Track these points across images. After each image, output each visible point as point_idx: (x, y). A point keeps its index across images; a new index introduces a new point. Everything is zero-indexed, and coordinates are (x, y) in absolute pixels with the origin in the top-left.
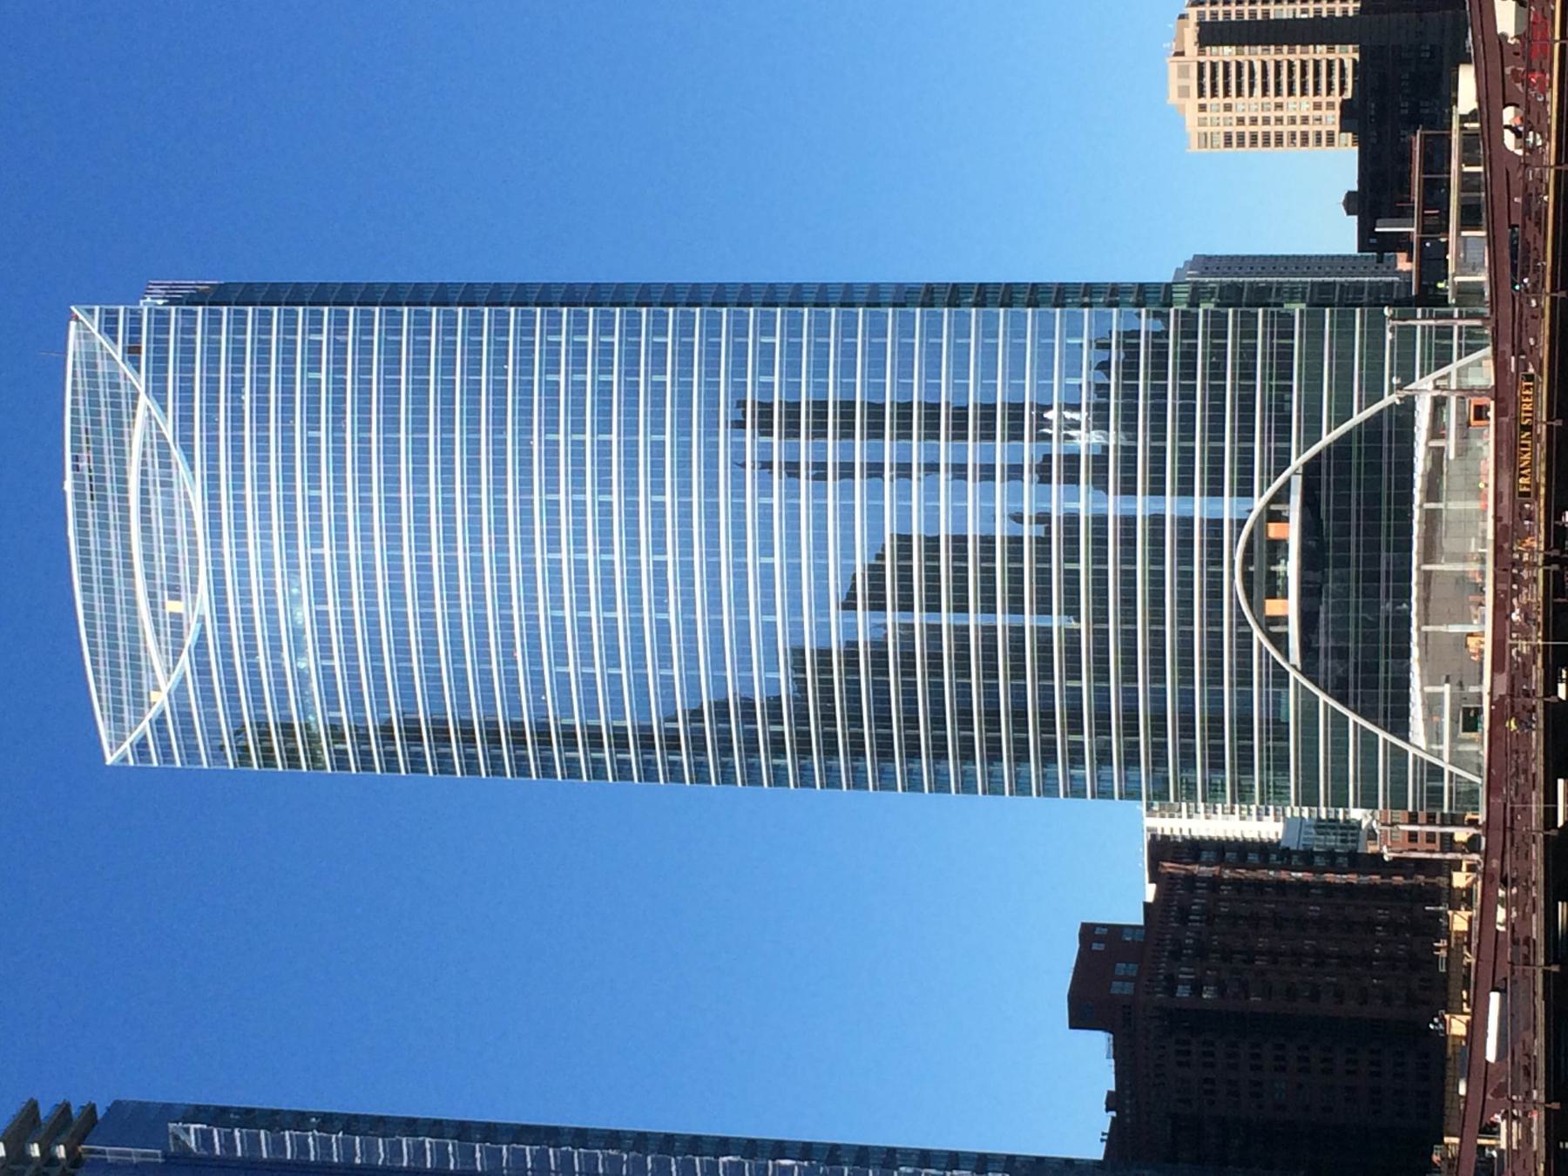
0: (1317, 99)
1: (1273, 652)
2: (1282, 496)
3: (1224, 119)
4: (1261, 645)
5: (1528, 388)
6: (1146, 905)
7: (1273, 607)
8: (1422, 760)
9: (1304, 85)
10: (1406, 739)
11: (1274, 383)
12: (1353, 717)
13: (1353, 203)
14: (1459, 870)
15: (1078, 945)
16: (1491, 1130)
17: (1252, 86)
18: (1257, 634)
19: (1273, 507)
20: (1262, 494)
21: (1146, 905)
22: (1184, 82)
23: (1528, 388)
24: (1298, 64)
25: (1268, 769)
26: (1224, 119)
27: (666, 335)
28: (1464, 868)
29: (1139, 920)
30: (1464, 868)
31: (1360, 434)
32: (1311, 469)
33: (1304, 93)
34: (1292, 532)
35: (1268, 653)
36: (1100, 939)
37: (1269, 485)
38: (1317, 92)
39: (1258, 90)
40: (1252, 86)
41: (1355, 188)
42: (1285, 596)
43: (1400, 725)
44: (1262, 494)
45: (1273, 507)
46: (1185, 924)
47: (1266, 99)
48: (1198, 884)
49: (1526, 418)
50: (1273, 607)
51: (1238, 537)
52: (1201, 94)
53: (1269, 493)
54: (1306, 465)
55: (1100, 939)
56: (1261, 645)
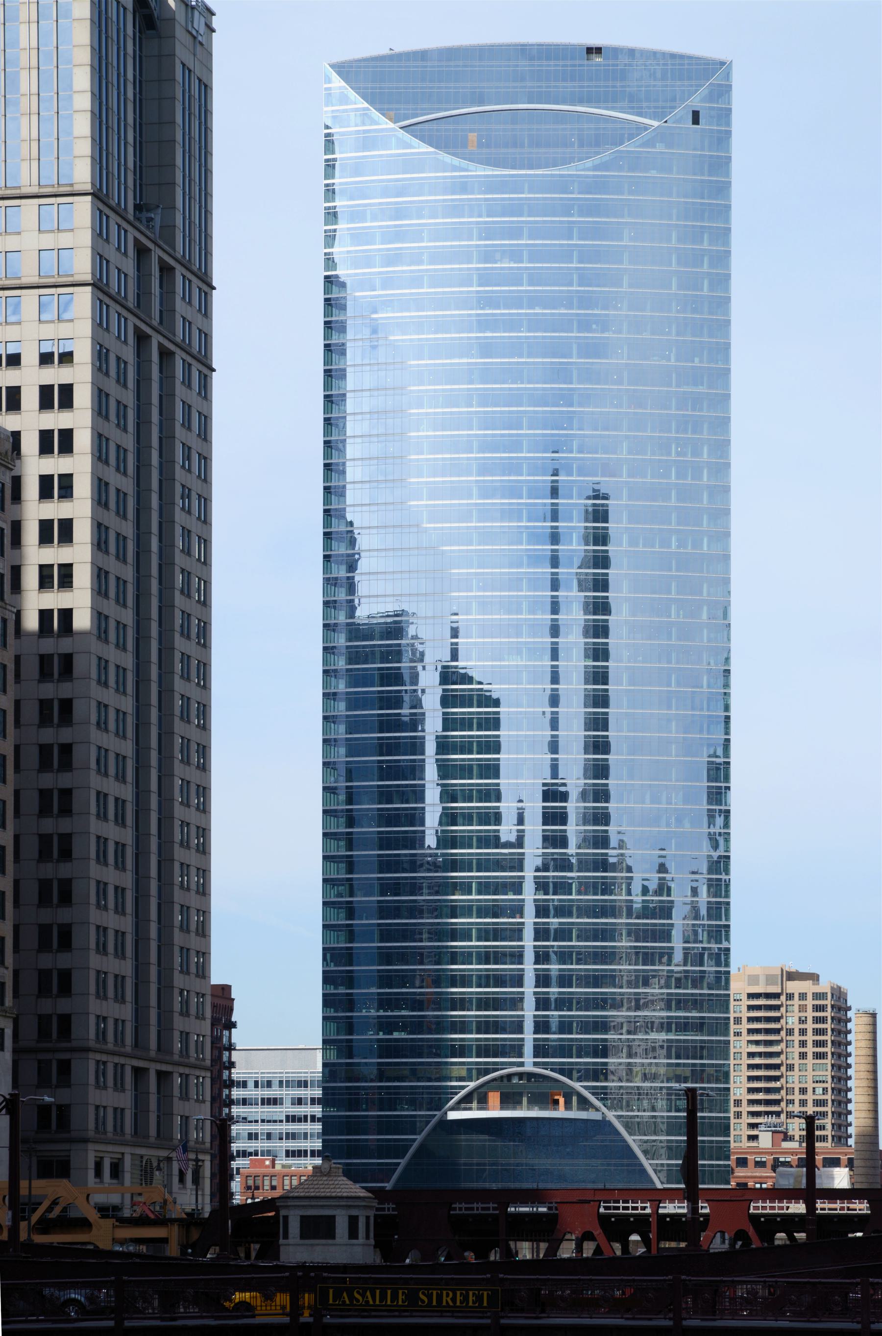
0: (745, 1103)
1: (457, 1098)
2: (584, 1103)
4: (463, 1087)
5: (479, 1298)
7: (494, 1098)
9: (757, 1090)
11: (673, 1097)
12: (403, 1162)
16: (618, 1290)
17: (757, 1043)
18: (472, 1085)
19: (575, 1099)
20: (586, 1088)
22: (762, 980)
23: (479, 1298)
24: (778, 1084)
25: (350, 1094)
27: (677, 570)
31: (635, 1165)
32: (604, 1125)
33: (751, 1090)
34: (561, 1113)
35: (456, 1094)
37: (593, 1094)
38: (751, 1102)
39: (754, 1049)
40: (757, 1043)
42: (502, 1108)
44: (586, 1088)
45: (575, 1099)
47: (745, 1056)
49: (430, 1297)
50: (494, 1098)
51: (552, 1070)
52: (751, 996)
53: (586, 1094)
54: (610, 1124)
56: (463, 1087)
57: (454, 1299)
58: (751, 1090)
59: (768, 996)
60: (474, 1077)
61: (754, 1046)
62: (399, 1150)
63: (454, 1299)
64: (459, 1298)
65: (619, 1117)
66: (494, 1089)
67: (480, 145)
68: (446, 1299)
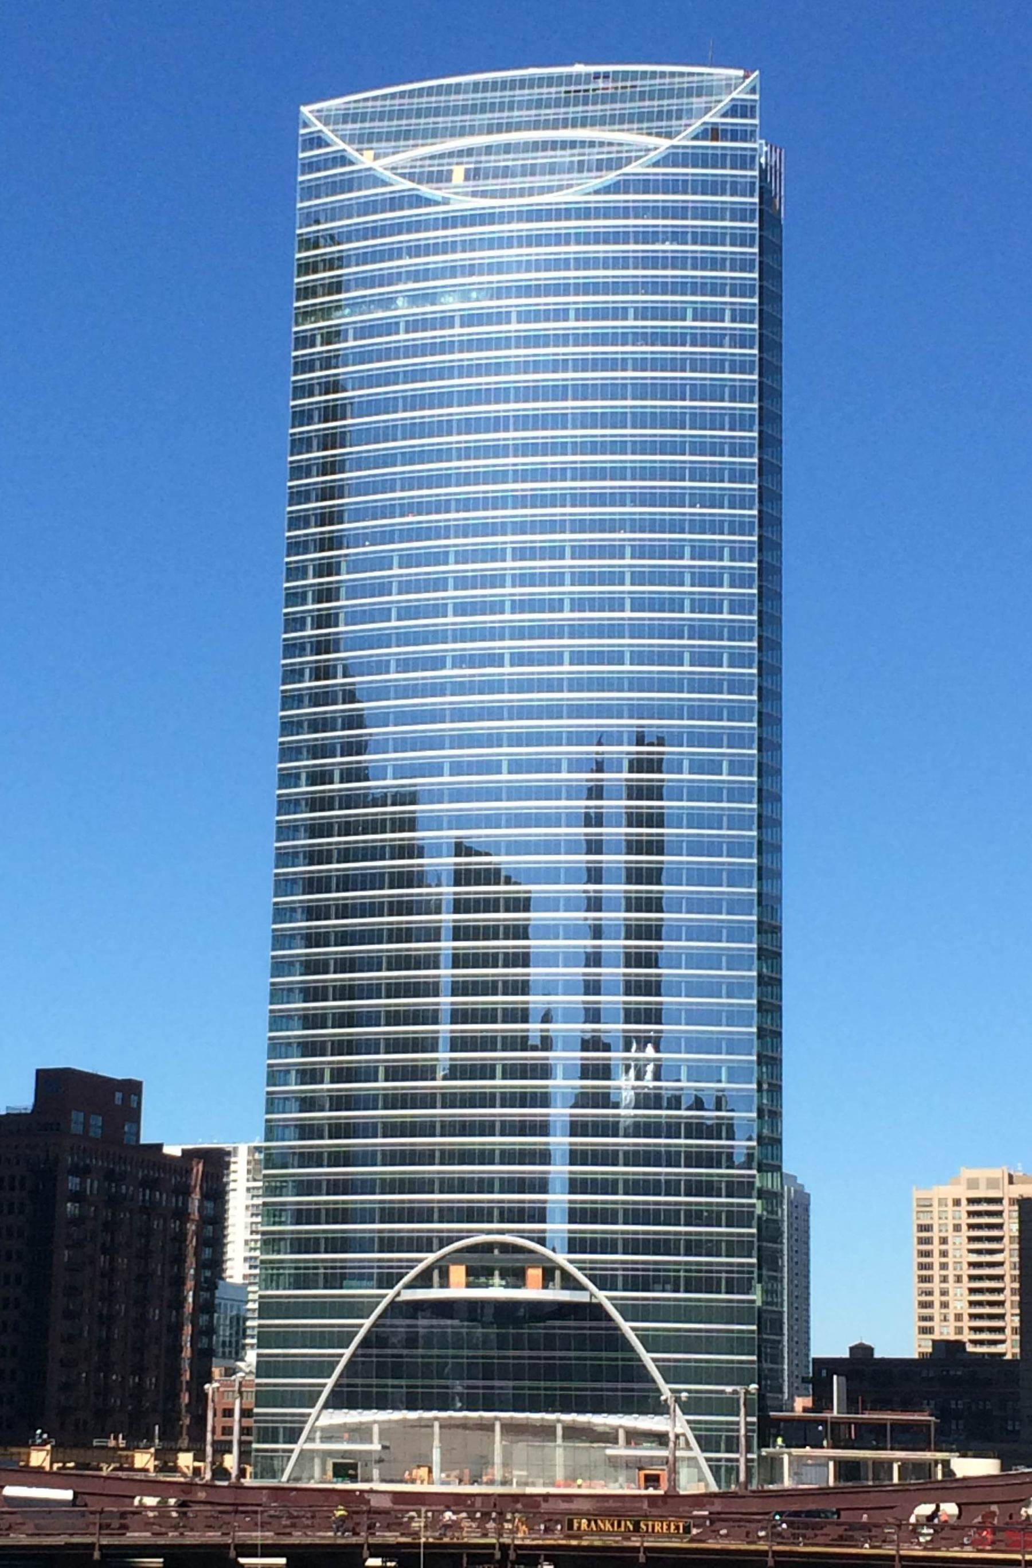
0: (966, 1317)
2: (569, 1282)
3: (946, 1225)
4: (420, 1261)
6: (159, 1147)
7: (458, 1273)
8: (305, 1422)
10: (326, 1406)
11: (682, 1274)
12: (348, 1352)
13: (862, 1353)
14: (195, 1459)
15: (120, 1077)
17: (979, 1252)
18: (430, 1257)
19: (558, 1273)
20: (571, 1262)
21: (159, 1147)
23: (677, 1528)
24: (1001, 1297)
26: (946, 1225)
28: (197, 1464)
29: (144, 1140)
30: (197, 1464)
32: (596, 1311)
33: (972, 1304)
36: (126, 1099)
37: (580, 1269)
38: (973, 1317)
39: (975, 1258)
40: (979, 1252)
41: (877, 1355)
42: (469, 1285)
43: (340, 1400)
44: (571, 1262)
45: (558, 1273)
46: (173, 1192)
48: (181, 1198)
49: (647, 1526)
50: (458, 1273)
52: (971, 1201)
53: (572, 1269)
55: (126, 1099)
56: (420, 1261)
57: (662, 1528)
58: (972, 1304)
59: (990, 1201)
60: (435, 1247)
61: (975, 1255)
62: (342, 1339)
63: (662, 1528)
64: (665, 1527)
65: (610, 1299)
66: (458, 1262)
67: (467, 178)
68: (657, 1528)
